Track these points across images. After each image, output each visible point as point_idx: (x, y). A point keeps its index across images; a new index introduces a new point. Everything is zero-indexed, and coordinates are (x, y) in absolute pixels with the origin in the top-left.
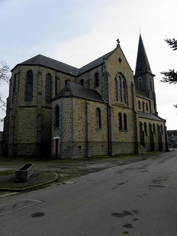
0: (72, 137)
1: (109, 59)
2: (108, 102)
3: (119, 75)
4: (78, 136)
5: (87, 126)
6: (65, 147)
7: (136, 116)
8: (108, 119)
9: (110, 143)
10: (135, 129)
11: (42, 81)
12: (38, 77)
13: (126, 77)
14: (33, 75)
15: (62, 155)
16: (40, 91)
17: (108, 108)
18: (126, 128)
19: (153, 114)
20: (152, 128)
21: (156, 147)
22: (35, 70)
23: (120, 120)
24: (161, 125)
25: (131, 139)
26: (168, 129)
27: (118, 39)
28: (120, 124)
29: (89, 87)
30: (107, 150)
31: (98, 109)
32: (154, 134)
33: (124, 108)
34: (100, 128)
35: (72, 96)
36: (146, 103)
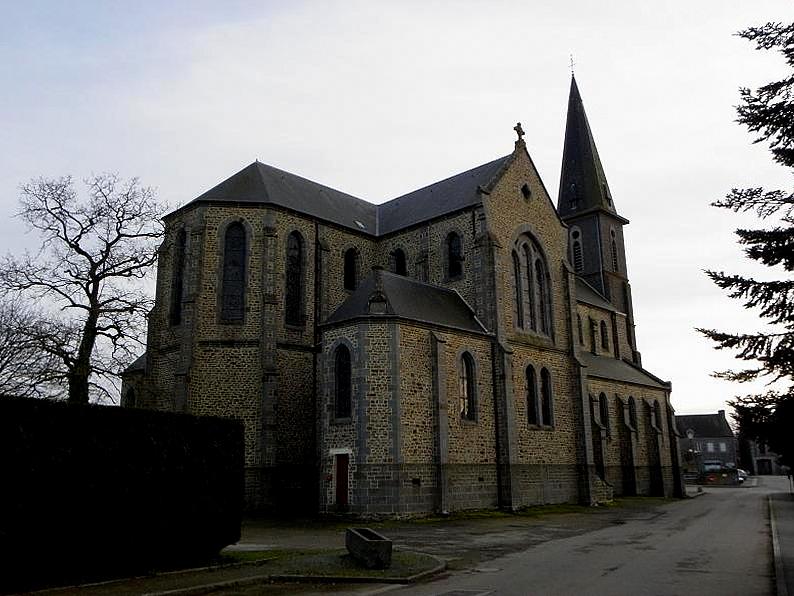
0: (394, 451)
1: (494, 193)
2: (496, 333)
4: (413, 449)
6: (371, 481)
8: (495, 390)
9: (503, 468)
10: (578, 421)
14: (244, 238)
15: (361, 509)
16: (270, 290)
17: (497, 352)
18: (548, 420)
19: (625, 361)
21: (642, 482)
22: (254, 220)
24: (631, 397)
25: (565, 457)
26: (676, 414)
27: (519, 124)
29: (426, 278)
30: (495, 491)
31: (467, 357)
32: (633, 434)
33: (542, 349)
35: (391, 319)
36: (599, 322)
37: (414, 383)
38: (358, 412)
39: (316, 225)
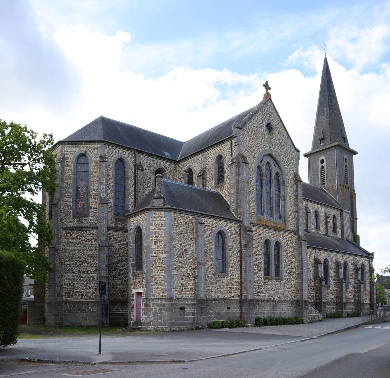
1: (246, 128)
3: (268, 159)
7: (301, 247)
8: (241, 254)
13: (283, 164)
16: (104, 195)
20: (341, 271)
23: (267, 254)
27: (267, 82)
28: (267, 263)
32: (344, 284)
33: (277, 229)
34: (224, 270)
36: (331, 217)
37: (182, 249)
38: (146, 266)
39: (135, 154)
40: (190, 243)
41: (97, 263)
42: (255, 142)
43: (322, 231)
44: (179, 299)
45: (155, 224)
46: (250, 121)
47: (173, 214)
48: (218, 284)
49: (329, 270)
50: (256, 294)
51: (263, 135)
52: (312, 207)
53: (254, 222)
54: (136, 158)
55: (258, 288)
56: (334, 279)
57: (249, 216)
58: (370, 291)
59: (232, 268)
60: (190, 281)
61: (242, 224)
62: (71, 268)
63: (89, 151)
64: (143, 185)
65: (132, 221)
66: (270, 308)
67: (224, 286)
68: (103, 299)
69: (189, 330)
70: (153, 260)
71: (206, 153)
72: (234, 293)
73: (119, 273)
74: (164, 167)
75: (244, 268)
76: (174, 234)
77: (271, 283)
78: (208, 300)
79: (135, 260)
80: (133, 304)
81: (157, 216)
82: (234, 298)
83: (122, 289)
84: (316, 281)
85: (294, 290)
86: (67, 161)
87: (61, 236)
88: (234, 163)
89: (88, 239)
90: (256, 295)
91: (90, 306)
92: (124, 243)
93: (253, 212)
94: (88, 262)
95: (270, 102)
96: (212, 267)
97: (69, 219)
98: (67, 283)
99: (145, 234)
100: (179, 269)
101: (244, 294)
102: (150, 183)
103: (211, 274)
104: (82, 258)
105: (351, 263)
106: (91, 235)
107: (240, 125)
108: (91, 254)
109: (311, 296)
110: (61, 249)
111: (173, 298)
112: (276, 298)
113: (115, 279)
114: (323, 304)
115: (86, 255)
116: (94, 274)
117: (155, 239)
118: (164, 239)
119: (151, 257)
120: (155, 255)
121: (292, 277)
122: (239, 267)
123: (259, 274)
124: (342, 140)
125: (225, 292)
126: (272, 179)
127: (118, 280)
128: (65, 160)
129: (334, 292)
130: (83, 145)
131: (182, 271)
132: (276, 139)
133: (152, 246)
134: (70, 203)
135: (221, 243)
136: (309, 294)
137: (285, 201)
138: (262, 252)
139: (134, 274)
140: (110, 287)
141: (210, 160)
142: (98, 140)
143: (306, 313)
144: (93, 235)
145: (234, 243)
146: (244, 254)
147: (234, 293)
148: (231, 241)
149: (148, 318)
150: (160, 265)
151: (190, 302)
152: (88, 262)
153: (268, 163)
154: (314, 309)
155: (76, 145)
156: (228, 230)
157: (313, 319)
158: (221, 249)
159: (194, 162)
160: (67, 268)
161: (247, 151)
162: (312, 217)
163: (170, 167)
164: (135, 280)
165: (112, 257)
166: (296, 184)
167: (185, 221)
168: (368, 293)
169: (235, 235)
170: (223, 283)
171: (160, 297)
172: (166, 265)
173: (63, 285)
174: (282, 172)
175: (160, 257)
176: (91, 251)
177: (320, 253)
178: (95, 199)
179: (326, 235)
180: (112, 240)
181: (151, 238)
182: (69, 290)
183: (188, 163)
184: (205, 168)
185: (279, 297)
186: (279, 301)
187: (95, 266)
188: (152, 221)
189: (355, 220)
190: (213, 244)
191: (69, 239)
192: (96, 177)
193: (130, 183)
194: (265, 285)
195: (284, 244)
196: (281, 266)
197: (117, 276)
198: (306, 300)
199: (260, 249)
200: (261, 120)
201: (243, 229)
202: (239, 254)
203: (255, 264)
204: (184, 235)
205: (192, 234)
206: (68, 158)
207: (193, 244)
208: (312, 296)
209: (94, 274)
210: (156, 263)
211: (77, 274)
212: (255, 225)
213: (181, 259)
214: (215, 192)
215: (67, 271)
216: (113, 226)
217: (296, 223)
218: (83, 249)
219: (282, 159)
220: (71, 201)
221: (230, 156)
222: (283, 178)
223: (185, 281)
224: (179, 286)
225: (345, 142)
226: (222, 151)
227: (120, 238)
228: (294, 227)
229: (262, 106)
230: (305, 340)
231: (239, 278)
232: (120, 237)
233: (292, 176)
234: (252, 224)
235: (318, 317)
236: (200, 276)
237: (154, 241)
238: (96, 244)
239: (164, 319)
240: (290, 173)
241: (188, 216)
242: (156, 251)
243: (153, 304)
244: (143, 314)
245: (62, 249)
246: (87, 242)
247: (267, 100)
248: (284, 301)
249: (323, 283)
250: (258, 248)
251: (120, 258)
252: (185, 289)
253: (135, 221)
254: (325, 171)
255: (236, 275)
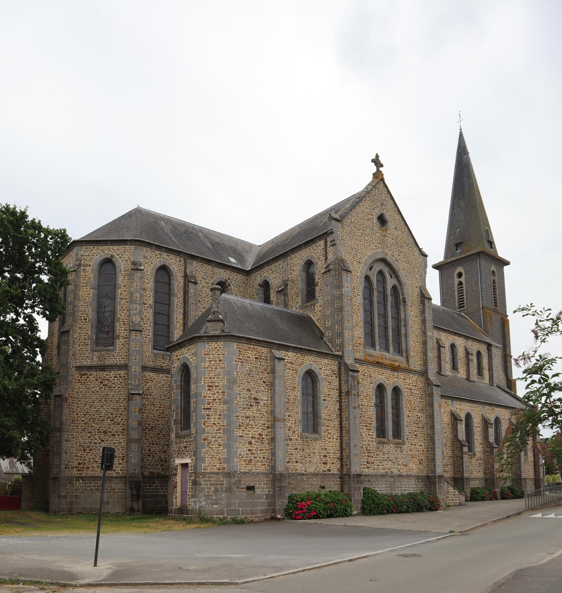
0: (228, 460)
1: (347, 221)
2: (343, 353)
3: (380, 266)
5: (273, 427)
7: (431, 395)
8: (340, 406)
11: (144, 289)
12: (130, 277)
13: (402, 274)
14: (115, 274)
18: (397, 433)
20: (491, 431)
23: (380, 406)
27: (377, 156)
29: (286, 305)
31: (310, 376)
33: (394, 369)
36: (475, 353)
37: (250, 398)
38: (196, 424)
39: (185, 260)
40: (263, 388)
41: (125, 420)
42: (360, 241)
43: (462, 373)
44: (246, 473)
45: (210, 360)
46: (353, 210)
47: (237, 345)
48: (305, 450)
49: (473, 429)
50: (365, 466)
51: (373, 230)
52: (447, 340)
53: (360, 357)
54: (187, 266)
55: (367, 457)
56: (480, 444)
57: (352, 349)
58: (534, 460)
59: (328, 426)
60: (263, 445)
61: (342, 361)
62: (87, 427)
63: (118, 255)
64: (196, 304)
65: (176, 355)
66: (387, 487)
67: (315, 453)
68: (133, 473)
69: (260, 522)
70: (205, 414)
71: (289, 258)
72: (331, 465)
73: (158, 434)
74: (229, 279)
75: (346, 427)
76: (238, 375)
77: (387, 450)
78: (291, 475)
79: (179, 414)
80: (176, 482)
81: (212, 348)
82: (330, 471)
83: (164, 458)
84: (454, 446)
85: (422, 460)
86: (85, 270)
87: (73, 378)
88: (329, 271)
89: (112, 384)
90: (364, 468)
91: (114, 484)
92: (167, 390)
93: (359, 344)
94: (112, 418)
95: (382, 184)
96: (297, 424)
97: (86, 353)
98: (81, 449)
99: (195, 376)
100: (246, 428)
101: (346, 465)
102: (207, 301)
103: (295, 436)
104: (104, 412)
105: (506, 420)
106: (117, 377)
107: (337, 216)
108: (117, 406)
109: (447, 469)
110: (72, 397)
111: (236, 472)
112: (395, 472)
113: (153, 444)
114: (465, 480)
115: (110, 406)
116: (121, 436)
117: (208, 383)
118: (223, 383)
119: (203, 409)
120: (209, 406)
121: (419, 441)
122: (337, 425)
123: (369, 435)
124: (487, 246)
125: (316, 463)
126: (387, 296)
127: (157, 444)
128: (82, 267)
129: (481, 462)
130: (108, 247)
131: (250, 431)
132: (392, 237)
133: (204, 393)
134: (88, 330)
135: (310, 391)
136: (444, 465)
137: (407, 328)
138: (372, 403)
139: (178, 436)
140: (145, 455)
141: (295, 268)
142: (130, 239)
143: (441, 494)
144: (120, 377)
145: (331, 389)
146: (346, 405)
147: (331, 465)
148: (326, 386)
149: (197, 503)
150: (216, 421)
151: (262, 477)
152: (112, 418)
153: (381, 272)
154: (452, 488)
155: (99, 247)
156: (320, 369)
157: (451, 503)
158: (310, 398)
159: (272, 272)
160: (82, 426)
161: (349, 253)
162: (446, 354)
163: (236, 279)
164: (178, 445)
165: (148, 410)
166: (423, 303)
167: (255, 355)
168: (532, 464)
169: (331, 376)
170: (313, 449)
171: (216, 471)
172: (225, 422)
173: (75, 451)
174: (401, 285)
175: (216, 409)
176: (117, 401)
177: (460, 405)
178: (124, 324)
179: (467, 379)
180: (149, 385)
181: (204, 380)
182: (83, 460)
183: (263, 274)
184: (288, 280)
185: (399, 471)
186: (400, 476)
187: (122, 424)
188: (205, 354)
189: (508, 358)
190: (298, 391)
191: (84, 383)
192: (126, 293)
193: (177, 302)
194: (378, 452)
195: (406, 390)
196: (401, 423)
197: (155, 438)
198: (441, 474)
199: (370, 398)
200: (370, 209)
201: (344, 368)
202: (338, 405)
203: (362, 421)
204: (253, 376)
205: (266, 374)
206: (86, 265)
207: (267, 390)
208: (449, 468)
209: (121, 436)
210: (211, 419)
211: (95, 435)
212: (362, 362)
213: (248, 413)
214: (302, 314)
215: (81, 430)
216: (151, 364)
217: (424, 360)
218: (105, 399)
219: (400, 266)
220: (89, 328)
221: (324, 261)
222: (403, 294)
223: (255, 446)
224: (245, 454)
225: (491, 248)
226: (313, 254)
227: (161, 382)
228: (421, 365)
229: (371, 190)
230: (440, 539)
231: (339, 441)
232: (160, 380)
233: (416, 292)
234: (357, 360)
235: (459, 500)
236: (278, 438)
237: (207, 385)
238: (124, 391)
239: (222, 504)
240: (413, 286)
241: (260, 347)
242: (211, 401)
243: (205, 481)
244: (190, 496)
245: (75, 398)
246: (111, 387)
247: (379, 181)
248: (408, 476)
249: (465, 449)
250: (366, 396)
251: (161, 412)
252: (254, 457)
253: (180, 355)
254: (464, 288)
255: (334, 437)
